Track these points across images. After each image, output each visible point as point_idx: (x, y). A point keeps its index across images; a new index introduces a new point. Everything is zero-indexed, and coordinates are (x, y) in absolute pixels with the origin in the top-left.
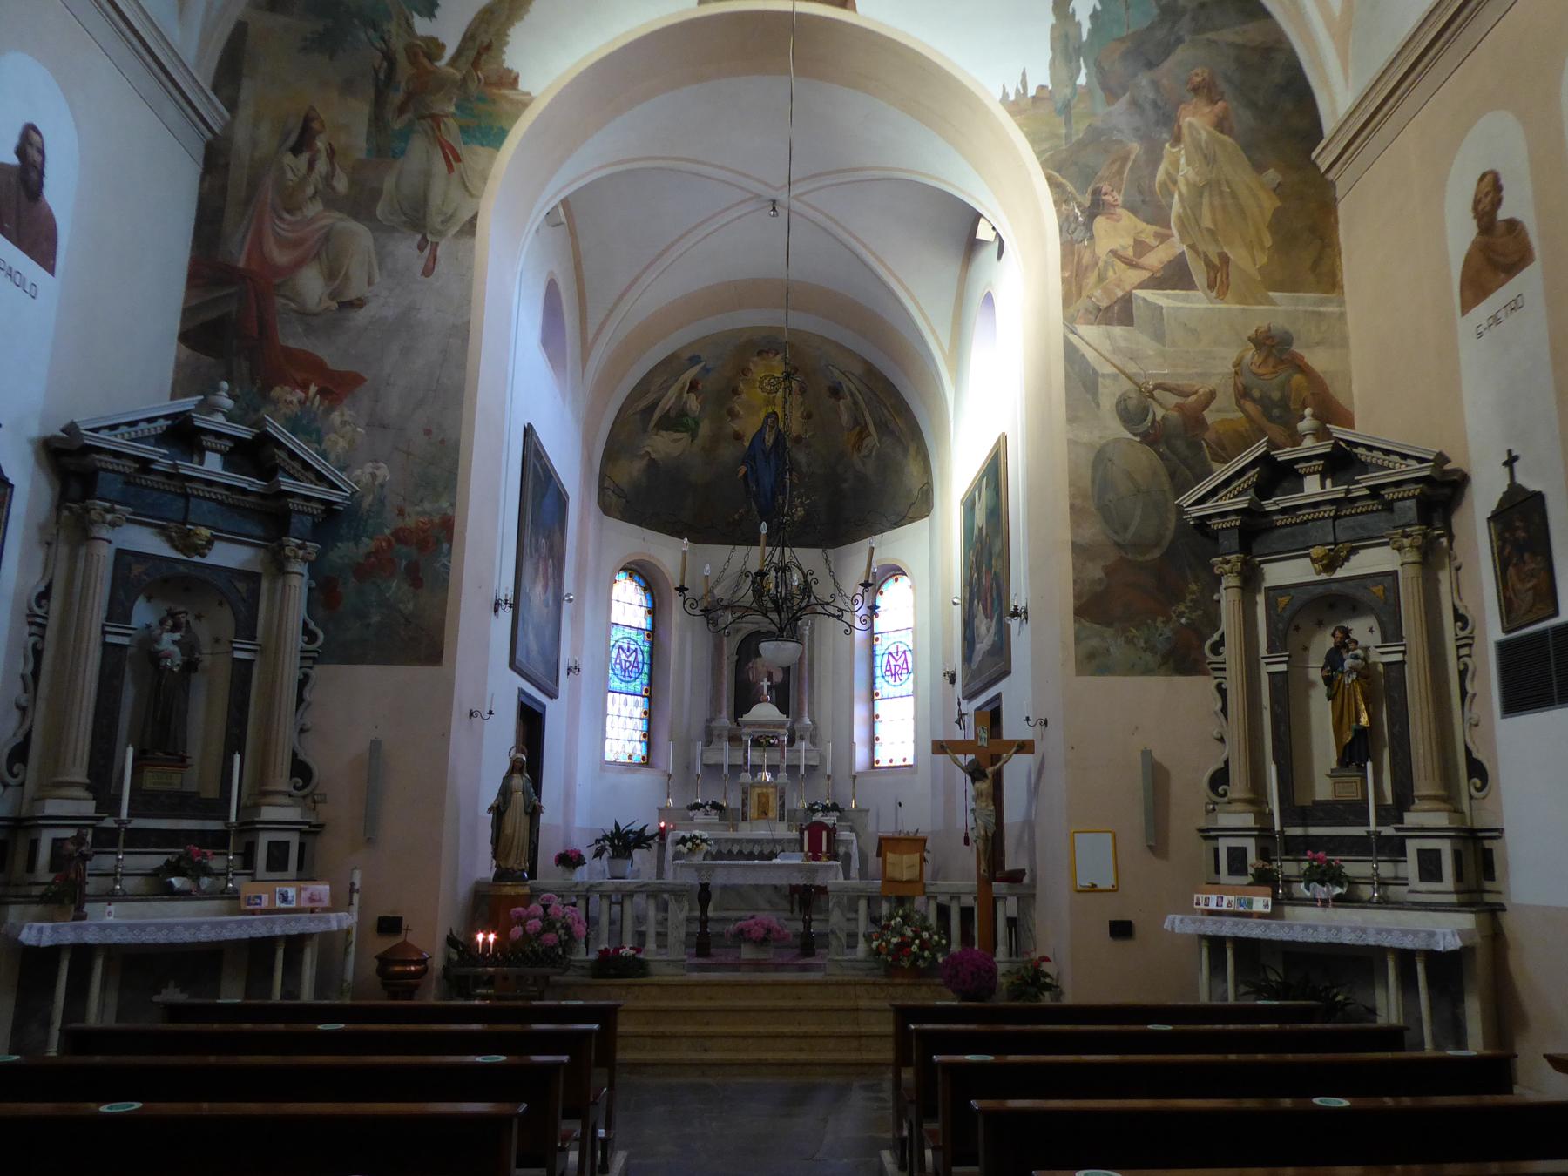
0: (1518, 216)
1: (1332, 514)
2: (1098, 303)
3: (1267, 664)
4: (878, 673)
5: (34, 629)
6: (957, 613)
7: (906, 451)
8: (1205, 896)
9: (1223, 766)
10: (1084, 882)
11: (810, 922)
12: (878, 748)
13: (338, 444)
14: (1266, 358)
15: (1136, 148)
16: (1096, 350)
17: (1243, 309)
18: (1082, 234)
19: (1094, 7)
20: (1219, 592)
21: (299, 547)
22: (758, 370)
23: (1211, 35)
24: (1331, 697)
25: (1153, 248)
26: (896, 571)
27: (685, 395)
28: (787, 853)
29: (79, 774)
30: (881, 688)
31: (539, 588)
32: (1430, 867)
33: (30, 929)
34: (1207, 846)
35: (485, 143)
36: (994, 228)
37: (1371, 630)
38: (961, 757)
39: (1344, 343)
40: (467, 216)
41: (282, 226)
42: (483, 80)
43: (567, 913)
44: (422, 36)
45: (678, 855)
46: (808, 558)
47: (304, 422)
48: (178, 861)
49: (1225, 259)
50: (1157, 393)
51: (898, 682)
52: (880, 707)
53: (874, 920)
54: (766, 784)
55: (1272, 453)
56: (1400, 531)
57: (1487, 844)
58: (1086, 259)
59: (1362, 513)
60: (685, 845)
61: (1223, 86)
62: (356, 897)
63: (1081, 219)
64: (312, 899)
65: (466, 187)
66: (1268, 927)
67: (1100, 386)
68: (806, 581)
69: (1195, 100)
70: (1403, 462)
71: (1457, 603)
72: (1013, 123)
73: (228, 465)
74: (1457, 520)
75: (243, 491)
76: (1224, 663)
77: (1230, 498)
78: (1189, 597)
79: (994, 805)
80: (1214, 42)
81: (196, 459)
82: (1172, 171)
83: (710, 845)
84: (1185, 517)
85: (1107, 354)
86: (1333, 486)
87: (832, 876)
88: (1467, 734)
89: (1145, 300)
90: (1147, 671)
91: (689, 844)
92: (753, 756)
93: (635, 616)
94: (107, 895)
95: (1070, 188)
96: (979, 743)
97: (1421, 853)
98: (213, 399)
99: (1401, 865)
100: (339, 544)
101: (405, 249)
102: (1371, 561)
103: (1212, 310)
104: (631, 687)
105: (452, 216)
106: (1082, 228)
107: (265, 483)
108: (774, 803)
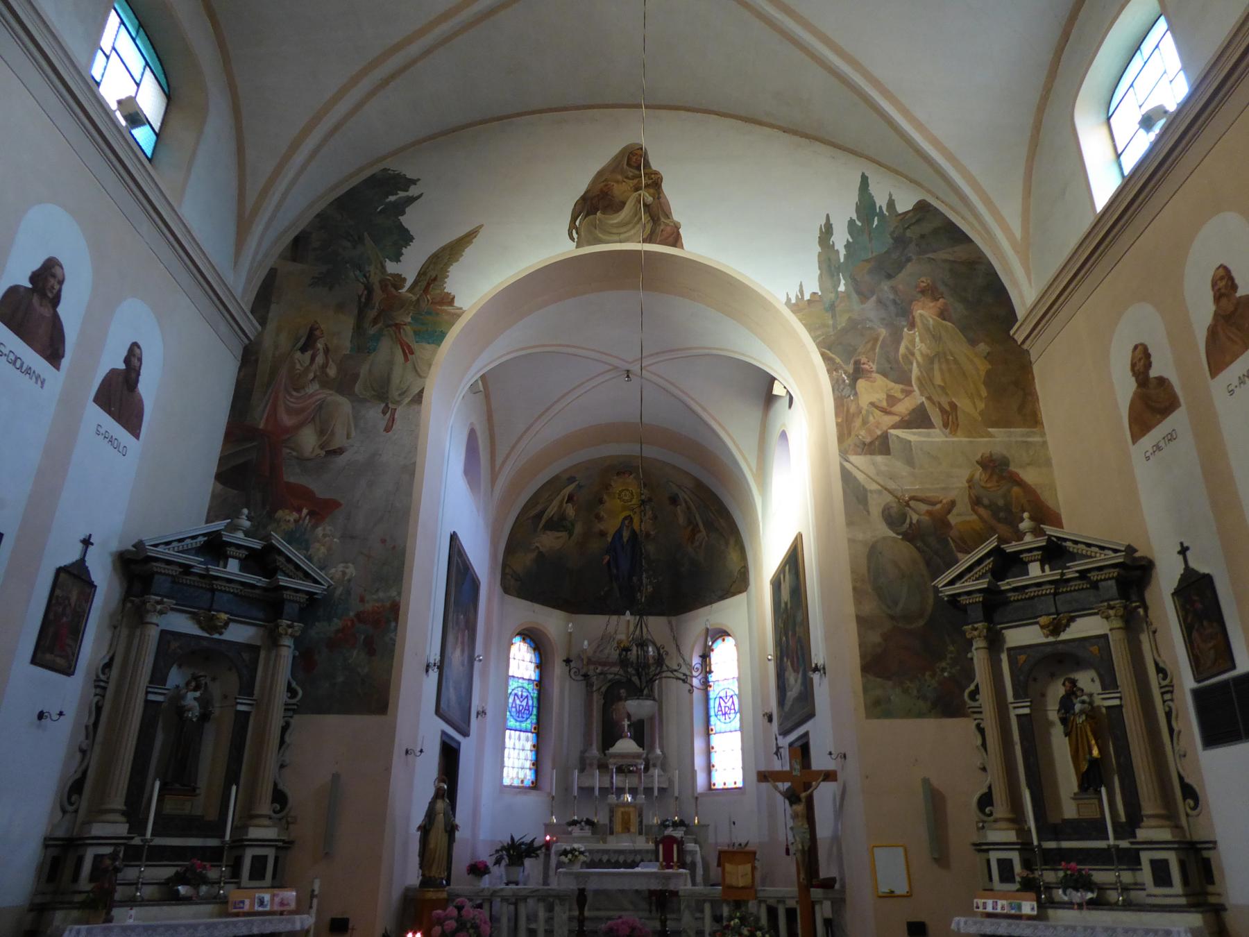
0: (1165, 375)
1: (1052, 591)
2: (864, 440)
3: (1015, 708)
4: (712, 713)
5: (98, 691)
6: (772, 667)
7: (727, 544)
8: (983, 901)
9: (987, 791)
10: (884, 889)
11: (666, 922)
12: (714, 774)
13: (320, 551)
14: (991, 475)
15: (883, 332)
16: (865, 474)
17: (971, 442)
18: (849, 391)
19: (848, 240)
20: (971, 651)
21: (289, 626)
22: (617, 485)
23: (930, 255)
24: (1067, 734)
25: (900, 400)
26: (722, 634)
27: (565, 505)
28: (646, 863)
29: (118, 802)
30: (715, 725)
31: (458, 652)
32: (1161, 874)
33: (71, 931)
34: (980, 858)
35: (430, 342)
36: (785, 387)
37: (1093, 680)
38: (780, 785)
39: (1048, 463)
40: (417, 391)
41: (292, 400)
42: (430, 301)
43: (476, 915)
44: (391, 274)
45: (560, 865)
46: (656, 625)
47: (298, 535)
48: (185, 871)
49: (954, 406)
50: (912, 503)
51: (728, 720)
52: (715, 740)
53: (717, 919)
54: (627, 804)
55: (1002, 546)
56: (1106, 604)
57: (1206, 854)
58: (853, 409)
59: (1075, 590)
60: (567, 857)
61: (942, 288)
62: (315, 901)
63: (847, 381)
64: (282, 904)
65: (416, 371)
66: (1036, 928)
67: (869, 498)
68: (659, 654)
69: (922, 299)
70: (1102, 552)
71: (1158, 659)
72: (795, 318)
73: (243, 568)
74: (1149, 595)
75: (253, 586)
76: (980, 707)
77: (973, 581)
78: (949, 656)
79: (808, 824)
80: (933, 259)
81: (222, 563)
82: (910, 347)
83: (586, 856)
84: (940, 595)
85: (873, 477)
86: (1051, 570)
87: (683, 883)
88: (1179, 765)
89: (898, 437)
90: (921, 715)
91: (570, 856)
92: (617, 780)
93: (527, 669)
94: (130, 901)
95: (838, 360)
96: (794, 773)
97: (1153, 863)
98: (236, 521)
99: (1138, 873)
100: (317, 624)
101: (373, 413)
102: (1086, 627)
103: (946, 441)
104: (524, 725)
105: (405, 392)
106: (848, 388)
107: (267, 580)
108: (634, 819)
